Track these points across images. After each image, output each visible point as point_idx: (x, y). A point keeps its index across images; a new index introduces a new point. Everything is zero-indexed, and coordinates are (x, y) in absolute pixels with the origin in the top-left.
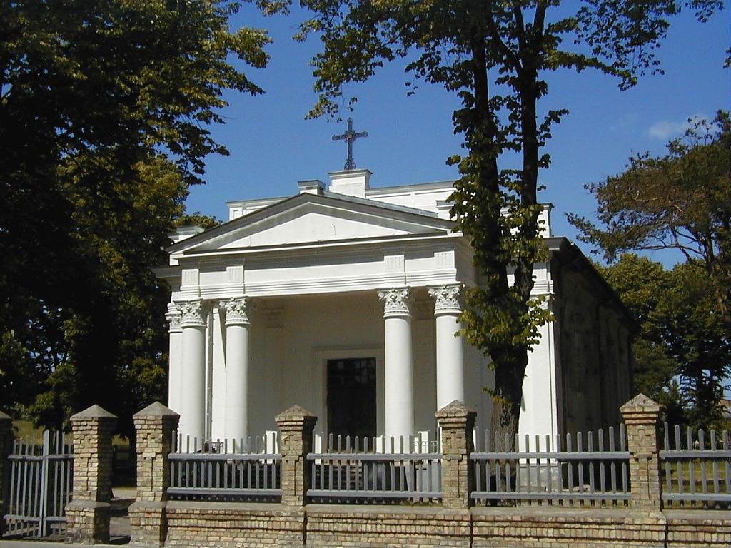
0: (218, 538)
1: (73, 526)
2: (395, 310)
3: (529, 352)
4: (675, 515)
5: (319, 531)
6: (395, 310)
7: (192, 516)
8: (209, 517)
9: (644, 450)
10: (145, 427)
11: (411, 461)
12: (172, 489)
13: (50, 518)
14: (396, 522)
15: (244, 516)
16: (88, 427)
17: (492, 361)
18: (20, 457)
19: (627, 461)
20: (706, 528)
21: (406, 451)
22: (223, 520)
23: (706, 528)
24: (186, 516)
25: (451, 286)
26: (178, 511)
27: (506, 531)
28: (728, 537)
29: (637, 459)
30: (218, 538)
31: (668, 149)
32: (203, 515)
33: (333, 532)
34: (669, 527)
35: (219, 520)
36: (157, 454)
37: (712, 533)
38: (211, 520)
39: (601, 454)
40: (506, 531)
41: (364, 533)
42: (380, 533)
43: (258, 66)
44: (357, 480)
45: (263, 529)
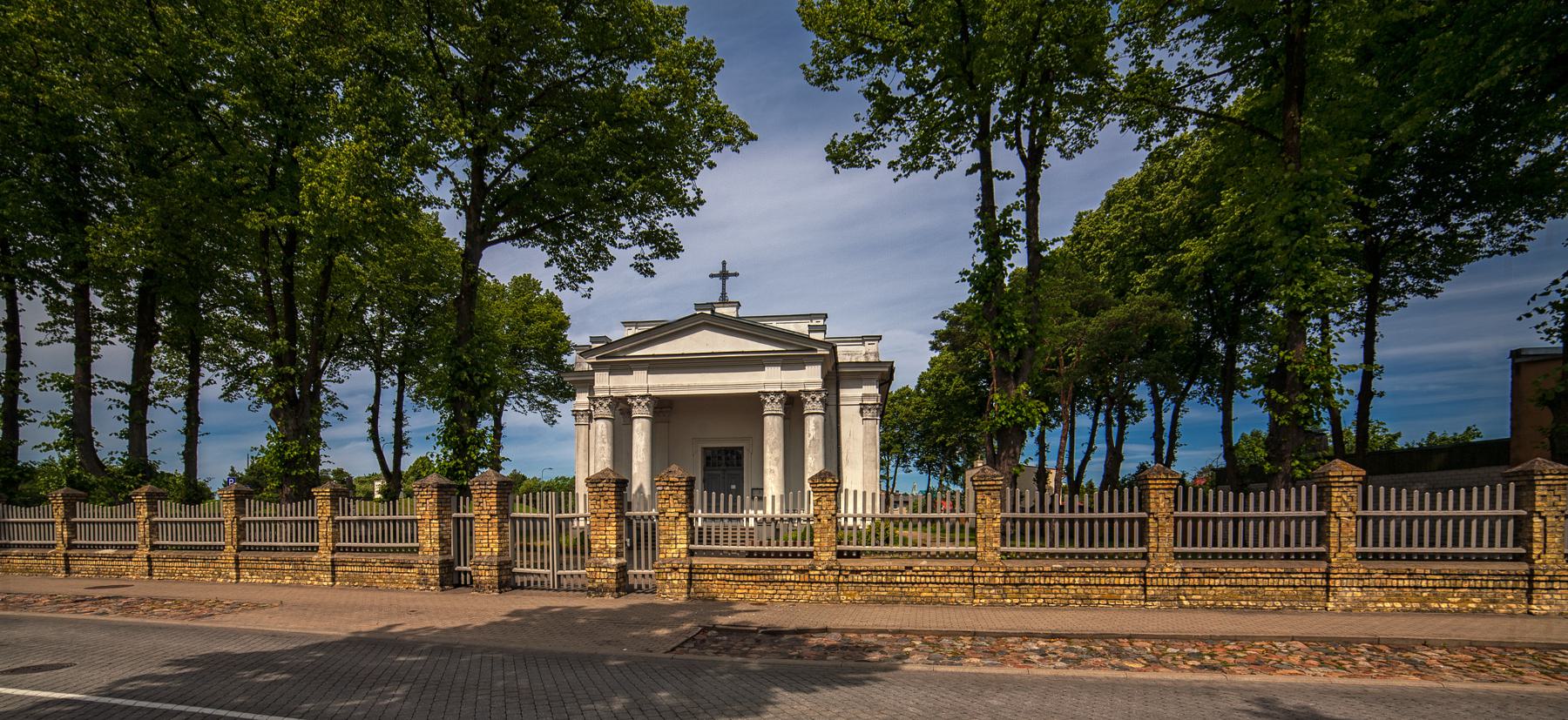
0: (745, 591)
1: (594, 581)
2: (773, 407)
3: (1400, 444)
4: (1190, 565)
5: (853, 582)
6: (773, 407)
7: (720, 571)
8: (738, 572)
9: (1164, 510)
10: (668, 488)
11: (756, 519)
12: (696, 546)
13: (560, 572)
14: (930, 573)
15: (774, 570)
16: (605, 489)
17: (199, 439)
18: (1231, 513)
19: (317, 521)
20: (1211, 575)
21: (869, 512)
22: (752, 575)
23: (1211, 575)
24: (713, 571)
25: (818, 392)
26: (704, 567)
27: (1036, 580)
28: (1566, 579)
29: (1156, 519)
30: (745, 591)
31: (567, 315)
32: (731, 570)
33: (867, 583)
34: (1184, 574)
35: (748, 575)
36: (680, 513)
37: (1215, 578)
38: (739, 574)
39: (347, 518)
40: (1036, 580)
41: (897, 583)
42: (913, 584)
43: (669, 257)
44: (721, 535)
45: (794, 582)
